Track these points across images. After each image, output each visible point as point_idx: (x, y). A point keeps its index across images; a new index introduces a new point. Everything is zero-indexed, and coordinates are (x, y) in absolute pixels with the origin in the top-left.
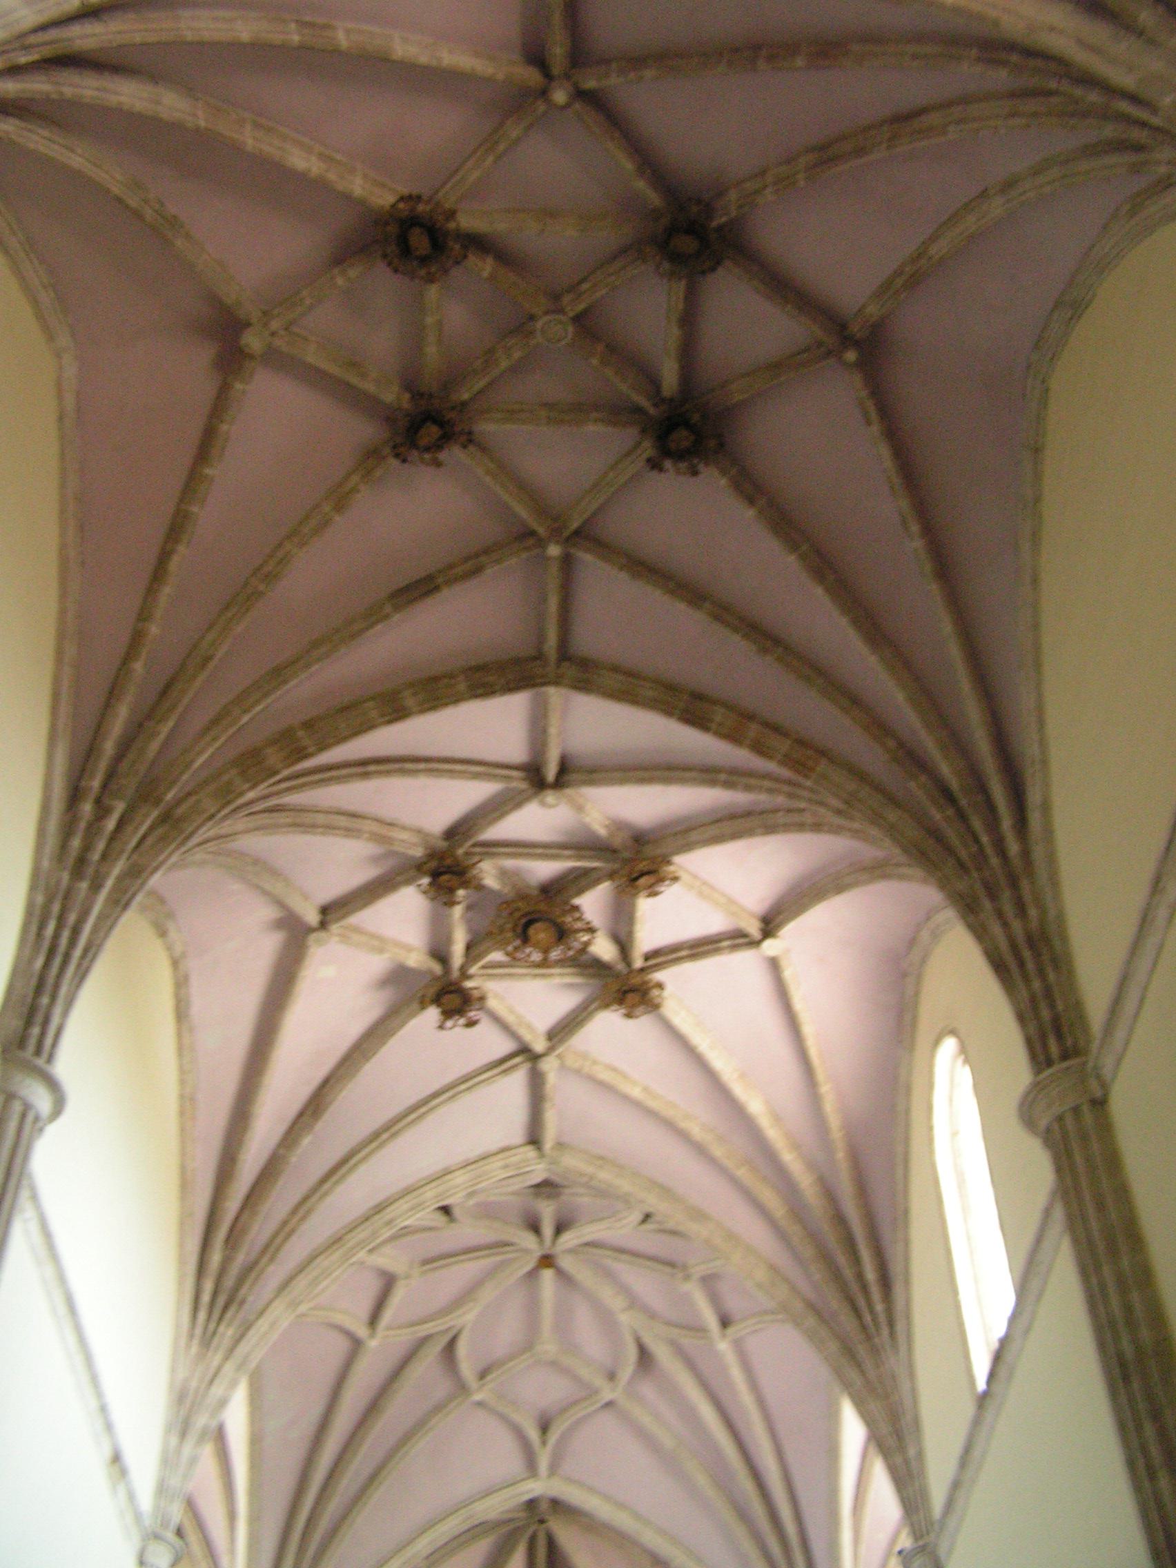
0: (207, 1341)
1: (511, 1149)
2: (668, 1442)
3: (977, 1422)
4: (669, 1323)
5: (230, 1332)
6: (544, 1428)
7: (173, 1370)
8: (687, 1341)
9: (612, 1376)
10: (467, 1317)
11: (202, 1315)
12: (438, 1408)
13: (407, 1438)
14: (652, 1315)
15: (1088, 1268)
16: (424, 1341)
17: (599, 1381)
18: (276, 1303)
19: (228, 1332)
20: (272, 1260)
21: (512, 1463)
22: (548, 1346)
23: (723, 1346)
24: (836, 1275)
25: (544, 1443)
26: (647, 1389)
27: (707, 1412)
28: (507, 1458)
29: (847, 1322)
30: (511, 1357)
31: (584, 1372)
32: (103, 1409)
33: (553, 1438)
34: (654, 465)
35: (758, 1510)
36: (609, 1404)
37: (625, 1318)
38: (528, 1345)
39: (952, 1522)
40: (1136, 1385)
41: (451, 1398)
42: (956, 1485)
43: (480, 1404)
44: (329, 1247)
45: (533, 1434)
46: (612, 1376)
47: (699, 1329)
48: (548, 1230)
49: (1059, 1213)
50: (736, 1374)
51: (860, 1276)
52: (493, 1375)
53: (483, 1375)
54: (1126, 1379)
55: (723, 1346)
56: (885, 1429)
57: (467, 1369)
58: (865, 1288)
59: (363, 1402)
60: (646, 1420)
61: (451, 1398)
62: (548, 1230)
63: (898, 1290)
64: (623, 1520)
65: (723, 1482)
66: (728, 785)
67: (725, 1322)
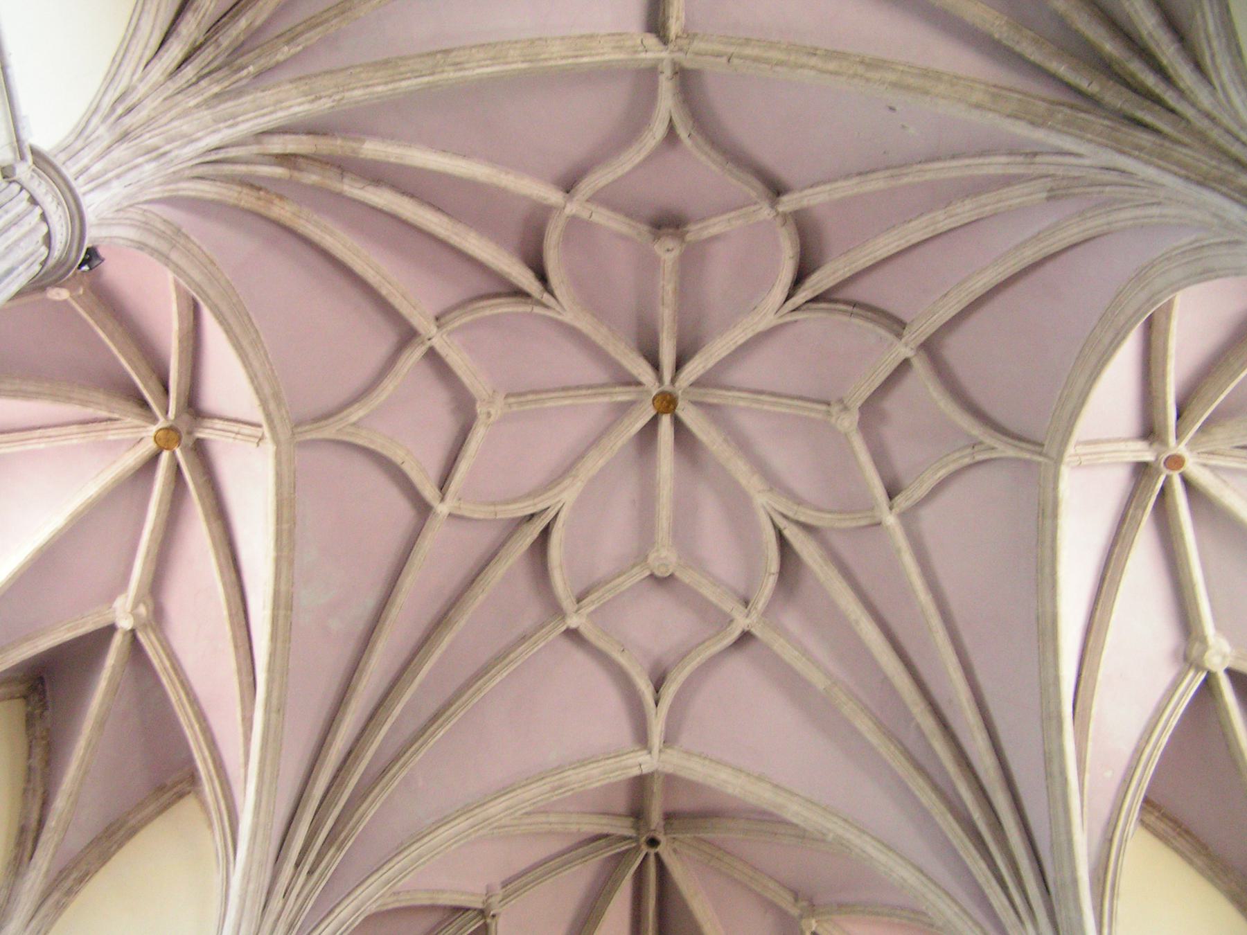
1: (1162, 291)
6: (658, 686)
9: (746, 603)
10: (567, 496)
17: (730, 605)
21: (619, 728)
26: (791, 620)
33: (670, 691)
34: (578, 627)
36: (746, 637)
44: (362, 394)
45: (645, 687)
46: (746, 603)
48: (667, 357)
62: (667, 357)
66: (343, 840)
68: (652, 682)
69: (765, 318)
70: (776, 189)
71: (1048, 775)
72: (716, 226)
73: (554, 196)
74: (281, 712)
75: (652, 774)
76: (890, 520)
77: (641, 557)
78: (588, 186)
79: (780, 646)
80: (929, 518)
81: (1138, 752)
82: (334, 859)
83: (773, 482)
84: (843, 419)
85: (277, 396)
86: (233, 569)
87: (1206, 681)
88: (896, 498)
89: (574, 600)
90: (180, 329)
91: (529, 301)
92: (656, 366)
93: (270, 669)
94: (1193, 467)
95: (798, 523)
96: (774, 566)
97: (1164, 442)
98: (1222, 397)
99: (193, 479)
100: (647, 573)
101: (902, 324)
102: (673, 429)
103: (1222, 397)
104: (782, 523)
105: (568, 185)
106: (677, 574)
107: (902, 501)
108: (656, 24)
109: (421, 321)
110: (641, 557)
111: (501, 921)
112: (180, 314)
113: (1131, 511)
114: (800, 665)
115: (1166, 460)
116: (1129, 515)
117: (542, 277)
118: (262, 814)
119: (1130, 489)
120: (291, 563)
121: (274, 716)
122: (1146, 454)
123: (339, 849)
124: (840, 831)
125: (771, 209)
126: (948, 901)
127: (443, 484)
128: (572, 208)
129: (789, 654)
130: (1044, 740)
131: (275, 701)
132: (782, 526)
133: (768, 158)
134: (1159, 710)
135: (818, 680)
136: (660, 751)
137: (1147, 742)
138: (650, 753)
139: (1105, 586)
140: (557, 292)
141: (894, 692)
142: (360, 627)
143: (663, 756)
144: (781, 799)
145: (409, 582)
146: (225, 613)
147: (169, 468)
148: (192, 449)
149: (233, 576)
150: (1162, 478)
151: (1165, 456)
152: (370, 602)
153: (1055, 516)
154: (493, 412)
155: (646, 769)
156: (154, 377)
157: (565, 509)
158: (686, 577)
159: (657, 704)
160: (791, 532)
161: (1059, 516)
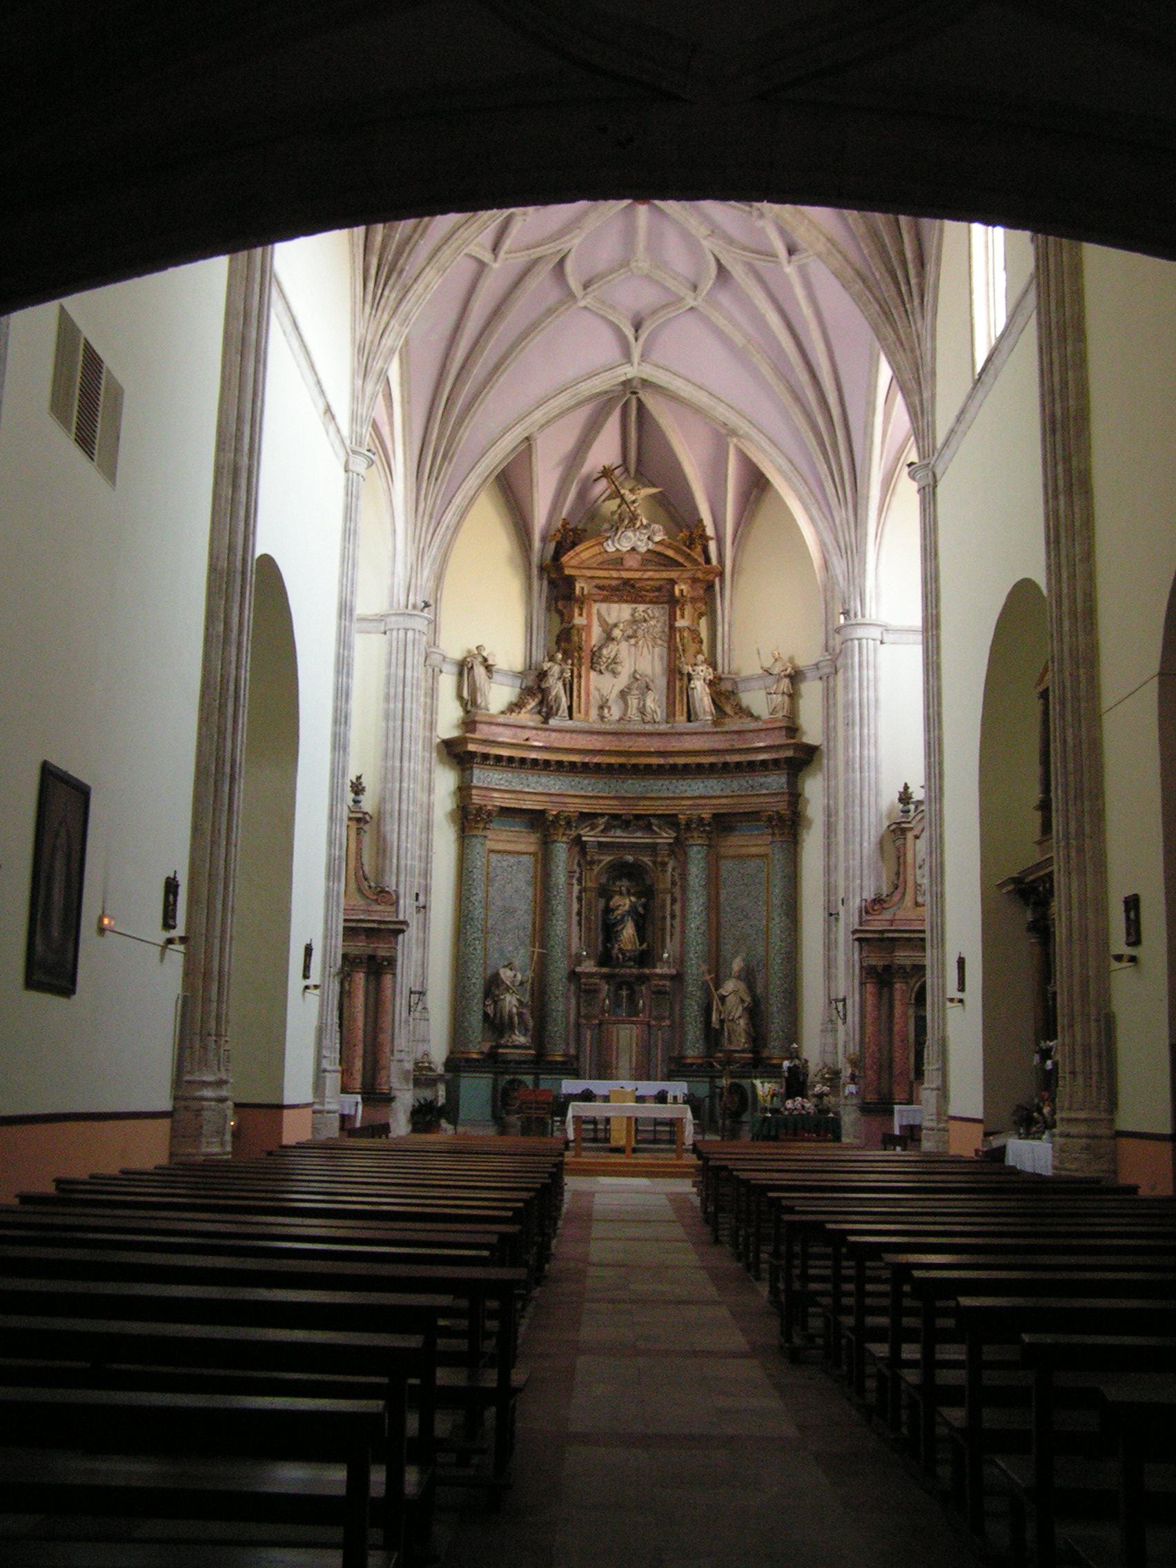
0: (376, 305)
2: (739, 340)
3: (970, 397)
4: (745, 249)
5: (393, 295)
6: (637, 328)
7: (354, 330)
8: (760, 265)
9: (695, 288)
10: (575, 242)
11: (371, 285)
12: (550, 312)
13: (524, 336)
14: (731, 241)
15: (1045, 349)
16: (535, 262)
17: (684, 291)
18: (428, 269)
19: (392, 295)
20: (421, 236)
22: (642, 262)
23: (790, 270)
24: (883, 252)
25: (636, 339)
26: (724, 298)
27: (773, 319)
28: (607, 350)
29: (889, 291)
30: (612, 271)
31: (670, 283)
32: (319, 383)
33: (644, 334)
35: (810, 396)
36: (692, 308)
37: (706, 244)
38: (625, 263)
39: (947, 453)
40: (1058, 437)
41: (561, 303)
42: (952, 431)
43: (585, 308)
45: (629, 332)
46: (695, 288)
47: (771, 255)
49: (1032, 298)
50: (800, 292)
51: (901, 253)
52: (595, 286)
53: (586, 286)
54: (1054, 431)
55: (790, 270)
56: (908, 375)
57: (574, 283)
58: (904, 262)
59: (487, 311)
60: (722, 323)
61: (561, 303)
63: (930, 267)
64: (702, 399)
65: (783, 372)
67: (791, 251)
71: (865, 433)
75: (633, 378)
82: (449, 469)
89: (581, 288)
111: (538, 441)
123: (450, 463)
124: (747, 429)
126: (802, 482)
138: (632, 365)
143: (641, 368)
144: (656, 657)
155: (629, 376)
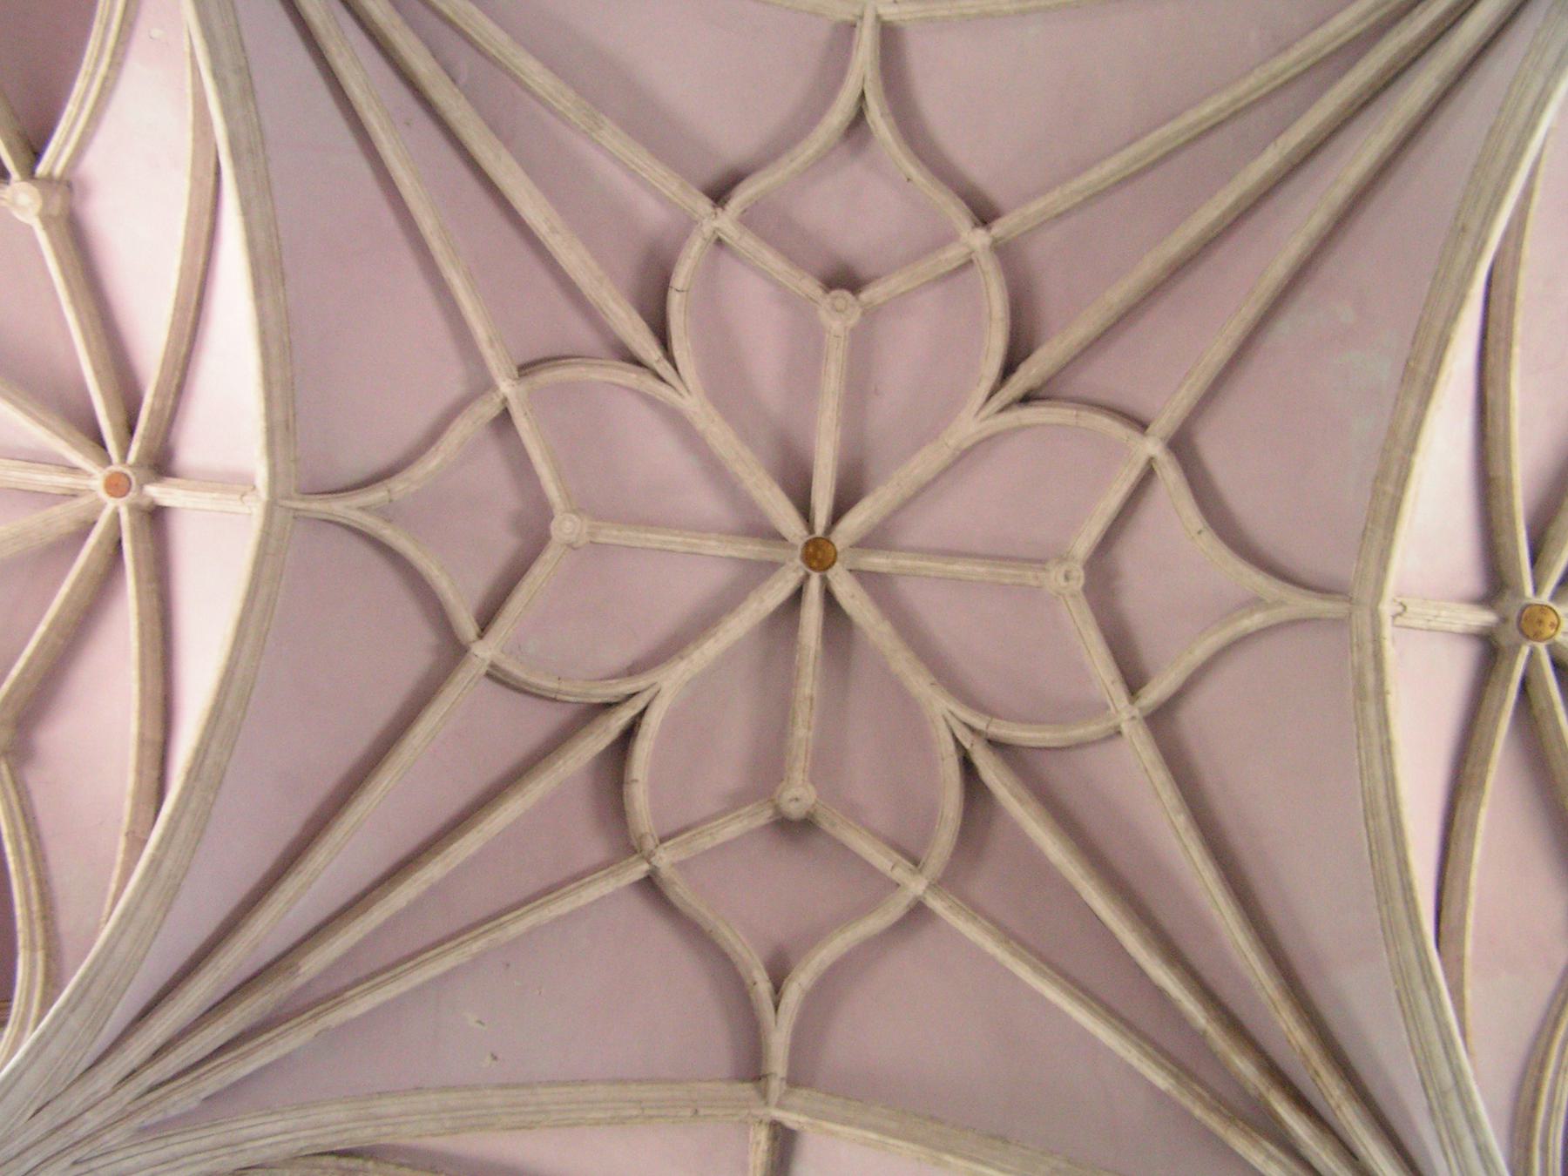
6: (858, 121)
9: (719, 242)
10: (968, 426)
26: (652, 214)
33: (838, 115)
45: (876, 115)
68: (868, 125)
69: (672, 681)
70: (651, 886)
71: (245, 71)
72: (732, 829)
73: (936, 904)
74: (1459, 225)
76: (506, 387)
77: (872, 315)
78: (895, 909)
79: (672, 186)
80: (453, 385)
81: (117, 64)
83: (677, 420)
84: (572, 533)
85: (1360, 695)
86: (1489, 402)
87: (37, 155)
88: (498, 412)
90: (1477, 806)
91: (989, 736)
92: (829, 598)
93: (1460, 299)
94: (97, 479)
95: (638, 362)
96: (675, 302)
97: (134, 509)
98: (65, 589)
99: (1516, 548)
100: (864, 296)
101: (488, 675)
102: (812, 502)
103: (65, 589)
104: (664, 368)
105: (918, 913)
106: (819, 292)
107: (487, 410)
108: (784, 1142)
109: (1140, 749)
110: (872, 315)
112: (1472, 836)
113: (170, 402)
114: (640, 158)
115: (129, 490)
116: (172, 396)
117: (968, 766)
118: (1535, 88)
119: (175, 430)
120: (1392, 432)
121: (1474, 225)
122: (159, 493)
125: (658, 866)
127: (1148, 476)
128: (916, 886)
129: (656, 172)
130: (257, 113)
131: (1467, 245)
132: (666, 363)
133: (660, 932)
134: (95, 118)
135: (612, 137)
136: (861, 18)
137: (106, 79)
138: (878, 17)
139: (195, 297)
140: (951, 747)
141: (494, 126)
142: (1306, 294)
143: (857, 11)
145: (1218, 351)
146: (1517, 350)
147: (1550, 566)
148: (1507, 587)
149: (1490, 394)
150: (132, 457)
151: (131, 494)
152: (1283, 328)
153: (270, 431)
154: (1061, 579)
156: (1536, 712)
157: (976, 408)
158: (809, 286)
159: (863, 96)
160: (647, 348)
161: (264, 430)
